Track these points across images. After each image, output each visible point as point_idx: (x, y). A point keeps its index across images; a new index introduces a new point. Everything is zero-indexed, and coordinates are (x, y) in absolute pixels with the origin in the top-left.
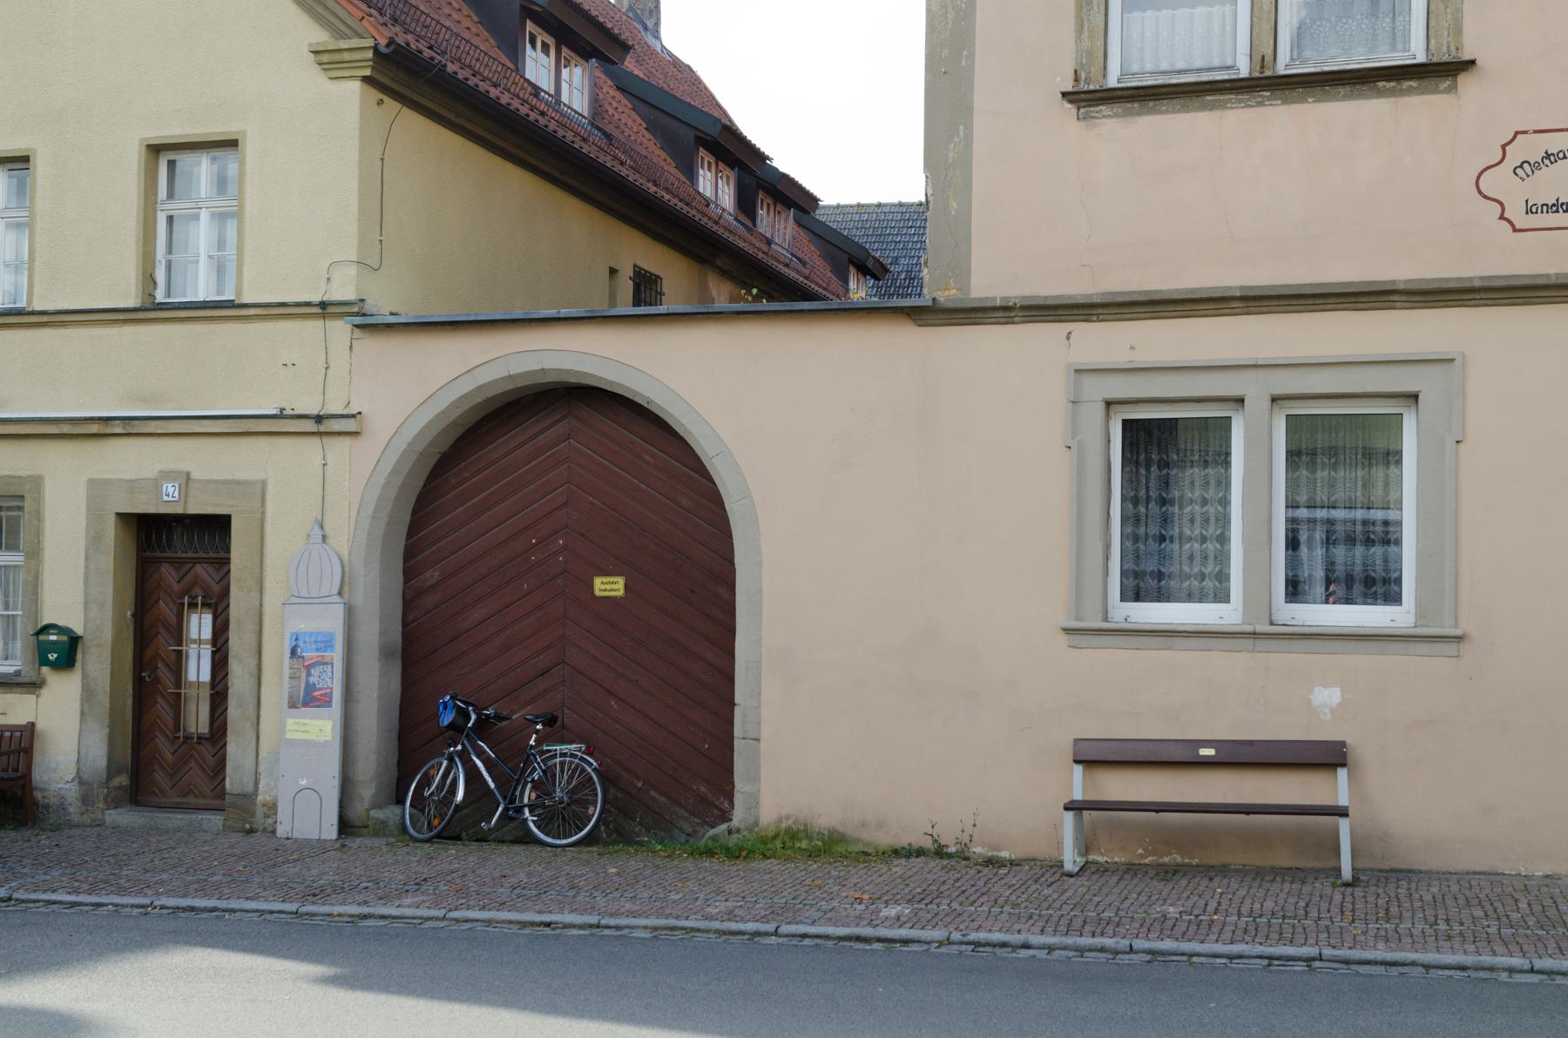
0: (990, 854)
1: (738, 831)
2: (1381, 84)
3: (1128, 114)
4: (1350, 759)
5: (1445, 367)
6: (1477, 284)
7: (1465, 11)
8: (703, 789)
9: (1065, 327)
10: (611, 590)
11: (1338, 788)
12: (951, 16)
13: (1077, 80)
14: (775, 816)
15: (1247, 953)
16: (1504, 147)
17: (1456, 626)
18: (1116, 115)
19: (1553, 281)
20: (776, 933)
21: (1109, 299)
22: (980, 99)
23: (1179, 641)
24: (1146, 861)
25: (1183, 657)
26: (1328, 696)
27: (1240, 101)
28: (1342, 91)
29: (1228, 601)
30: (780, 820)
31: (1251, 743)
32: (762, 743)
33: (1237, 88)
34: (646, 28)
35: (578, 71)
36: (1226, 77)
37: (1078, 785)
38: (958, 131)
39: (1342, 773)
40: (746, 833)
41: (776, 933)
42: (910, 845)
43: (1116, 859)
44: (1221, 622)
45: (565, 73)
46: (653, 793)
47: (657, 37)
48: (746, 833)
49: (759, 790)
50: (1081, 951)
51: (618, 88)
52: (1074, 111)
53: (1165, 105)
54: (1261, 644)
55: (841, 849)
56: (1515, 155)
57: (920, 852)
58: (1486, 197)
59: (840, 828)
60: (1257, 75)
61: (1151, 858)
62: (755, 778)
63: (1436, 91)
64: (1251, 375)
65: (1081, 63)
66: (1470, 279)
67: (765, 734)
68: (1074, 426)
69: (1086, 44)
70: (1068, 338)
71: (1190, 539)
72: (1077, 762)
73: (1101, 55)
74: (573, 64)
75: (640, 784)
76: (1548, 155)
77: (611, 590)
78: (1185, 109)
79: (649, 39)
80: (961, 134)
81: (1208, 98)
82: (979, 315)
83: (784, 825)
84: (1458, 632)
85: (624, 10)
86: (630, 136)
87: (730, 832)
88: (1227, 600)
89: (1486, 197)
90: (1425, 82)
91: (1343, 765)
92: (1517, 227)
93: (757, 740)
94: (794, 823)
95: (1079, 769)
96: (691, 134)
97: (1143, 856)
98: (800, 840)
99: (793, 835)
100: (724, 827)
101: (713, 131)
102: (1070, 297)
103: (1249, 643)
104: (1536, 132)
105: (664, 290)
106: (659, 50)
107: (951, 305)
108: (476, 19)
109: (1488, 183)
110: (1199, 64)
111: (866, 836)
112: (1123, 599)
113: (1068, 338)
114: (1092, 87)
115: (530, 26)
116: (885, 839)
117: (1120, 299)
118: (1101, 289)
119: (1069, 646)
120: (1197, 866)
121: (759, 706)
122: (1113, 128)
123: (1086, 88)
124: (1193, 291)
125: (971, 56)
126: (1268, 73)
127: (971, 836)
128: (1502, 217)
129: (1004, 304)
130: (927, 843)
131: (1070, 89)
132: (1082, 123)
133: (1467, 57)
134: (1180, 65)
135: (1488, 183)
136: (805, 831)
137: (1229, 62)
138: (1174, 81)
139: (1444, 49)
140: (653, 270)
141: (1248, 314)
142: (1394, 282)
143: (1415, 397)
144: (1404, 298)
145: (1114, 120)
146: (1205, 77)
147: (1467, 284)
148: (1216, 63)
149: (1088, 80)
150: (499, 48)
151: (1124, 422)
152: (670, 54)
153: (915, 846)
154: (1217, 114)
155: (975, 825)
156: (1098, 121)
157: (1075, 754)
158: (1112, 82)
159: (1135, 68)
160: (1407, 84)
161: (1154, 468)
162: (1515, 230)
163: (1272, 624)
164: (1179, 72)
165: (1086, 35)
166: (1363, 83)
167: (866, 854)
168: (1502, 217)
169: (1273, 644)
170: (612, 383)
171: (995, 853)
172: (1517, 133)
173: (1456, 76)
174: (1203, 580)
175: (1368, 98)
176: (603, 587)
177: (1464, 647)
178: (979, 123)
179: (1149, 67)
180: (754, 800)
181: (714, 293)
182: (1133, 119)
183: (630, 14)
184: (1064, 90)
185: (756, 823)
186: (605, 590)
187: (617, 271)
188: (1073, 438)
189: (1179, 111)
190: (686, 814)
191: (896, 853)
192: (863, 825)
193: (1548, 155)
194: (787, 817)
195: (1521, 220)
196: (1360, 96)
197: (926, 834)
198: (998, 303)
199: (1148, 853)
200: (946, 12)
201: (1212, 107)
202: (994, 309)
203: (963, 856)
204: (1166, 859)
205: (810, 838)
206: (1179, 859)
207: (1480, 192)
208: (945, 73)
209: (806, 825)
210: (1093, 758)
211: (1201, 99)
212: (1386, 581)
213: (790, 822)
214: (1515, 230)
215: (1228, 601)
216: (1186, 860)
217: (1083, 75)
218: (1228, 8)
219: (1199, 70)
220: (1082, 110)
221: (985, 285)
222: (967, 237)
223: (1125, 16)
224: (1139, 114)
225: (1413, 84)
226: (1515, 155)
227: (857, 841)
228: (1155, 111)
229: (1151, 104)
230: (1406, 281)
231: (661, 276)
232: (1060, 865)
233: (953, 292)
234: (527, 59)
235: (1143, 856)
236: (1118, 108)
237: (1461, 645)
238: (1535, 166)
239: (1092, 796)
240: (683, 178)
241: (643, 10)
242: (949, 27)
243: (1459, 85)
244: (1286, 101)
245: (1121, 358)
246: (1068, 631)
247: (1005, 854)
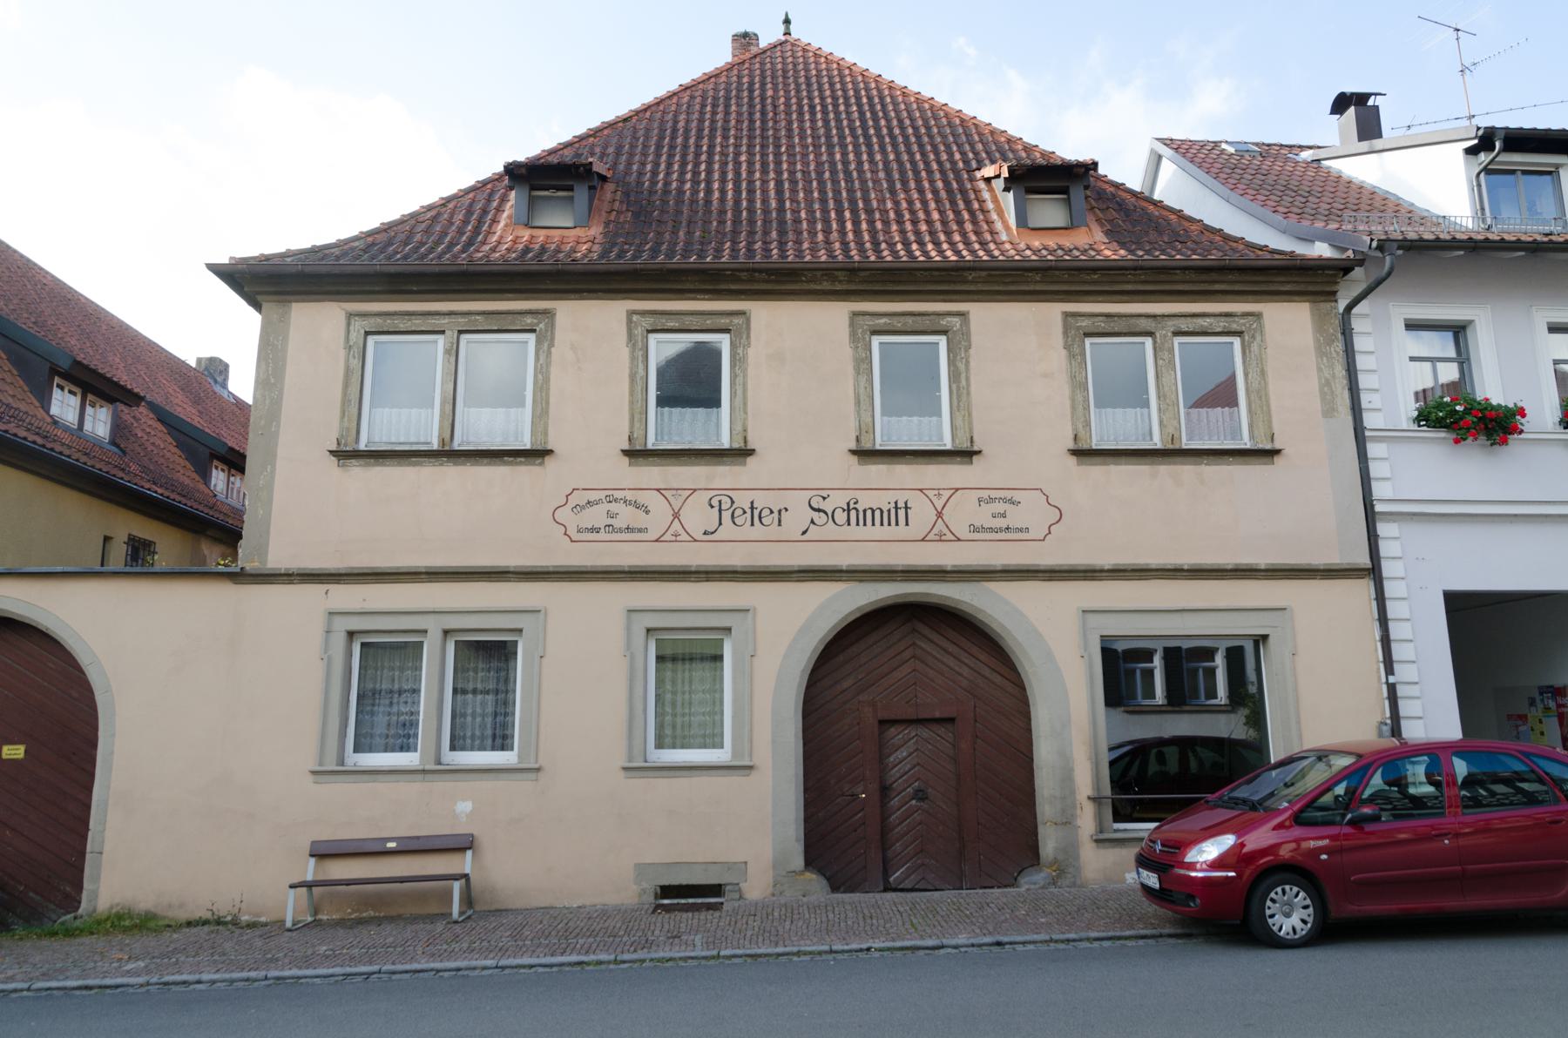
0: (253, 920)
1: (81, 917)
2: (506, 458)
3: (367, 465)
4: (475, 844)
5: (535, 615)
6: (551, 569)
7: (550, 424)
8: (68, 889)
9: (325, 587)
10: (15, 754)
11: (465, 864)
12: (267, 402)
13: (338, 444)
14: (108, 905)
15: (337, 973)
16: (567, 496)
17: (536, 762)
18: (360, 465)
19: (589, 569)
20: (29, 989)
21: (349, 571)
22: (281, 452)
23: (380, 777)
24: (353, 917)
25: (382, 787)
26: (465, 807)
27: (430, 462)
28: (485, 461)
29: (722, 747)
30: (112, 907)
31: (418, 838)
32: (104, 855)
33: (429, 455)
34: (216, 381)
35: (104, 410)
36: (426, 449)
37: (310, 870)
38: (266, 469)
39: (469, 853)
40: (86, 918)
41: (29, 989)
42: (200, 918)
43: (334, 917)
44: (412, 764)
45: (89, 410)
46: (31, 894)
47: (224, 385)
48: (86, 918)
49: (98, 888)
50: (232, 981)
51: (159, 420)
52: (336, 462)
53: (388, 461)
54: (429, 777)
55: (152, 924)
56: (573, 501)
57: (206, 922)
58: (557, 522)
59: (153, 910)
60: (441, 449)
61: (355, 915)
62: (96, 879)
63: (534, 464)
64: (431, 618)
65: (342, 435)
66: (547, 567)
67: (107, 848)
68: (327, 646)
69: (346, 424)
70: (326, 593)
71: (403, 714)
72: (312, 856)
73: (354, 432)
74: (98, 406)
75: (22, 888)
76: (589, 502)
77: (15, 754)
78: (400, 465)
79: (218, 389)
80: (268, 470)
81: (414, 459)
82: (272, 578)
83: (114, 911)
84: (536, 766)
85: (201, 370)
86: (152, 451)
87: (75, 918)
88: (722, 747)
89: (557, 522)
90: (529, 459)
91: (470, 848)
92: (573, 539)
93: (101, 853)
94: (122, 908)
95: (312, 861)
96: (208, 451)
97: (350, 914)
98: (124, 920)
99: (120, 917)
100: (71, 916)
101: (223, 451)
102: (326, 569)
103: (420, 777)
104: (625, 489)
105: (156, 550)
106: (226, 396)
107: (253, 572)
108: (15, 372)
109: (559, 515)
110: (413, 439)
111: (170, 914)
112: (656, 748)
113: (326, 593)
114: (348, 449)
115: (57, 380)
116: (183, 916)
117: (356, 571)
118: (346, 566)
119: (314, 783)
120: (383, 917)
121: (104, 830)
122: (360, 475)
123: (344, 449)
124: (398, 568)
125: (278, 426)
126: (447, 448)
127: (240, 909)
128: (565, 534)
129: (286, 572)
130: (208, 915)
131: (335, 449)
132: (341, 469)
133: (549, 448)
134: (402, 440)
135: (559, 515)
136: (129, 913)
137: (429, 441)
138: (397, 449)
139: (539, 443)
140: (147, 538)
141: (431, 582)
142: (508, 567)
143: (729, 629)
144: (514, 576)
145: (358, 468)
146: (414, 448)
147: (546, 570)
148: (422, 440)
149: (346, 445)
150: (31, 392)
151: (456, 641)
152: (235, 397)
153: (204, 917)
154: (417, 468)
155: (242, 902)
156: (349, 468)
157: (311, 851)
158: (362, 447)
159: (377, 439)
160: (519, 459)
161: (385, 671)
162: (572, 541)
163: (646, 761)
164: (400, 443)
165: (346, 419)
166: (496, 457)
167: (169, 926)
168: (565, 534)
169: (436, 776)
170: (21, 616)
171: (256, 919)
172: (574, 490)
173: (544, 457)
174: (409, 738)
175: (499, 465)
176: (9, 752)
177: (540, 774)
178: (280, 464)
179: (384, 439)
180: (95, 895)
181: (206, 552)
182: (370, 468)
183: (206, 373)
184: (331, 449)
185: (95, 911)
186: (10, 754)
187: (111, 538)
188: (325, 653)
189: (396, 466)
190: (54, 907)
191: (189, 924)
192: (170, 906)
193: (589, 502)
194: (118, 905)
195: (575, 536)
196: (495, 465)
197: (208, 910)
198: (283, 572)
199: (354, 911)
200: (265, 399)
201: (415, 464)
202: (281, 575)
203: (235, 923)
204: (364, 915)
205: (131, 918)
206: (372, 913)
207: (555, 520)
208: (262, 434)
209: (129, 910)
210: (322, 853)
211: (409, 460)
212: (714, 735)
213: (119, 908)
214: (572, 541)
215: (722, 747)
216: (377, 914)
217: (343, 442)
218: (430, 410)
219: (412, 443)
220: (341, 461)
221: (277, 560)
222: (268, 532)
223: (373, 410)
224: (373, 465)
225: (523, 459)
226: (573, 501)
227: (164, 918)
228: (383, 465)
229: (381, 460)
230: (515, 567)
231: (154, 540)
232: (283, 922)
233: (256, 564)
234: (54, 401)
235: (350, 914)
236: (362, 462)
237: (539, 774)
238: (583, 508)
239: (321, 877)
240: (197, 478)
241: (214, 371)
242: (266, 407)
243: (546, 462)
244: (455, 464)
245: (357, 607)
246: (314, 773)
247: (263, 919)
